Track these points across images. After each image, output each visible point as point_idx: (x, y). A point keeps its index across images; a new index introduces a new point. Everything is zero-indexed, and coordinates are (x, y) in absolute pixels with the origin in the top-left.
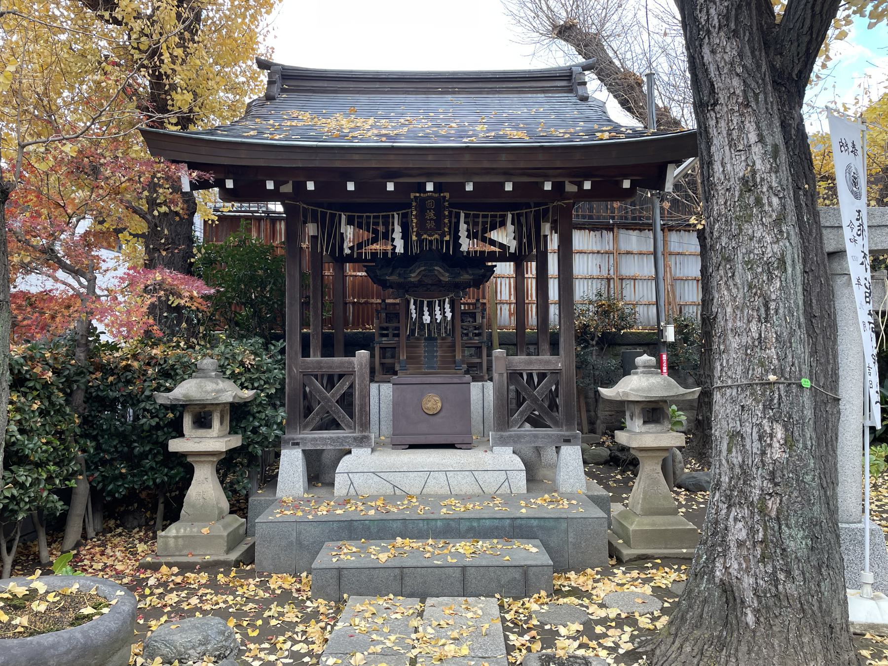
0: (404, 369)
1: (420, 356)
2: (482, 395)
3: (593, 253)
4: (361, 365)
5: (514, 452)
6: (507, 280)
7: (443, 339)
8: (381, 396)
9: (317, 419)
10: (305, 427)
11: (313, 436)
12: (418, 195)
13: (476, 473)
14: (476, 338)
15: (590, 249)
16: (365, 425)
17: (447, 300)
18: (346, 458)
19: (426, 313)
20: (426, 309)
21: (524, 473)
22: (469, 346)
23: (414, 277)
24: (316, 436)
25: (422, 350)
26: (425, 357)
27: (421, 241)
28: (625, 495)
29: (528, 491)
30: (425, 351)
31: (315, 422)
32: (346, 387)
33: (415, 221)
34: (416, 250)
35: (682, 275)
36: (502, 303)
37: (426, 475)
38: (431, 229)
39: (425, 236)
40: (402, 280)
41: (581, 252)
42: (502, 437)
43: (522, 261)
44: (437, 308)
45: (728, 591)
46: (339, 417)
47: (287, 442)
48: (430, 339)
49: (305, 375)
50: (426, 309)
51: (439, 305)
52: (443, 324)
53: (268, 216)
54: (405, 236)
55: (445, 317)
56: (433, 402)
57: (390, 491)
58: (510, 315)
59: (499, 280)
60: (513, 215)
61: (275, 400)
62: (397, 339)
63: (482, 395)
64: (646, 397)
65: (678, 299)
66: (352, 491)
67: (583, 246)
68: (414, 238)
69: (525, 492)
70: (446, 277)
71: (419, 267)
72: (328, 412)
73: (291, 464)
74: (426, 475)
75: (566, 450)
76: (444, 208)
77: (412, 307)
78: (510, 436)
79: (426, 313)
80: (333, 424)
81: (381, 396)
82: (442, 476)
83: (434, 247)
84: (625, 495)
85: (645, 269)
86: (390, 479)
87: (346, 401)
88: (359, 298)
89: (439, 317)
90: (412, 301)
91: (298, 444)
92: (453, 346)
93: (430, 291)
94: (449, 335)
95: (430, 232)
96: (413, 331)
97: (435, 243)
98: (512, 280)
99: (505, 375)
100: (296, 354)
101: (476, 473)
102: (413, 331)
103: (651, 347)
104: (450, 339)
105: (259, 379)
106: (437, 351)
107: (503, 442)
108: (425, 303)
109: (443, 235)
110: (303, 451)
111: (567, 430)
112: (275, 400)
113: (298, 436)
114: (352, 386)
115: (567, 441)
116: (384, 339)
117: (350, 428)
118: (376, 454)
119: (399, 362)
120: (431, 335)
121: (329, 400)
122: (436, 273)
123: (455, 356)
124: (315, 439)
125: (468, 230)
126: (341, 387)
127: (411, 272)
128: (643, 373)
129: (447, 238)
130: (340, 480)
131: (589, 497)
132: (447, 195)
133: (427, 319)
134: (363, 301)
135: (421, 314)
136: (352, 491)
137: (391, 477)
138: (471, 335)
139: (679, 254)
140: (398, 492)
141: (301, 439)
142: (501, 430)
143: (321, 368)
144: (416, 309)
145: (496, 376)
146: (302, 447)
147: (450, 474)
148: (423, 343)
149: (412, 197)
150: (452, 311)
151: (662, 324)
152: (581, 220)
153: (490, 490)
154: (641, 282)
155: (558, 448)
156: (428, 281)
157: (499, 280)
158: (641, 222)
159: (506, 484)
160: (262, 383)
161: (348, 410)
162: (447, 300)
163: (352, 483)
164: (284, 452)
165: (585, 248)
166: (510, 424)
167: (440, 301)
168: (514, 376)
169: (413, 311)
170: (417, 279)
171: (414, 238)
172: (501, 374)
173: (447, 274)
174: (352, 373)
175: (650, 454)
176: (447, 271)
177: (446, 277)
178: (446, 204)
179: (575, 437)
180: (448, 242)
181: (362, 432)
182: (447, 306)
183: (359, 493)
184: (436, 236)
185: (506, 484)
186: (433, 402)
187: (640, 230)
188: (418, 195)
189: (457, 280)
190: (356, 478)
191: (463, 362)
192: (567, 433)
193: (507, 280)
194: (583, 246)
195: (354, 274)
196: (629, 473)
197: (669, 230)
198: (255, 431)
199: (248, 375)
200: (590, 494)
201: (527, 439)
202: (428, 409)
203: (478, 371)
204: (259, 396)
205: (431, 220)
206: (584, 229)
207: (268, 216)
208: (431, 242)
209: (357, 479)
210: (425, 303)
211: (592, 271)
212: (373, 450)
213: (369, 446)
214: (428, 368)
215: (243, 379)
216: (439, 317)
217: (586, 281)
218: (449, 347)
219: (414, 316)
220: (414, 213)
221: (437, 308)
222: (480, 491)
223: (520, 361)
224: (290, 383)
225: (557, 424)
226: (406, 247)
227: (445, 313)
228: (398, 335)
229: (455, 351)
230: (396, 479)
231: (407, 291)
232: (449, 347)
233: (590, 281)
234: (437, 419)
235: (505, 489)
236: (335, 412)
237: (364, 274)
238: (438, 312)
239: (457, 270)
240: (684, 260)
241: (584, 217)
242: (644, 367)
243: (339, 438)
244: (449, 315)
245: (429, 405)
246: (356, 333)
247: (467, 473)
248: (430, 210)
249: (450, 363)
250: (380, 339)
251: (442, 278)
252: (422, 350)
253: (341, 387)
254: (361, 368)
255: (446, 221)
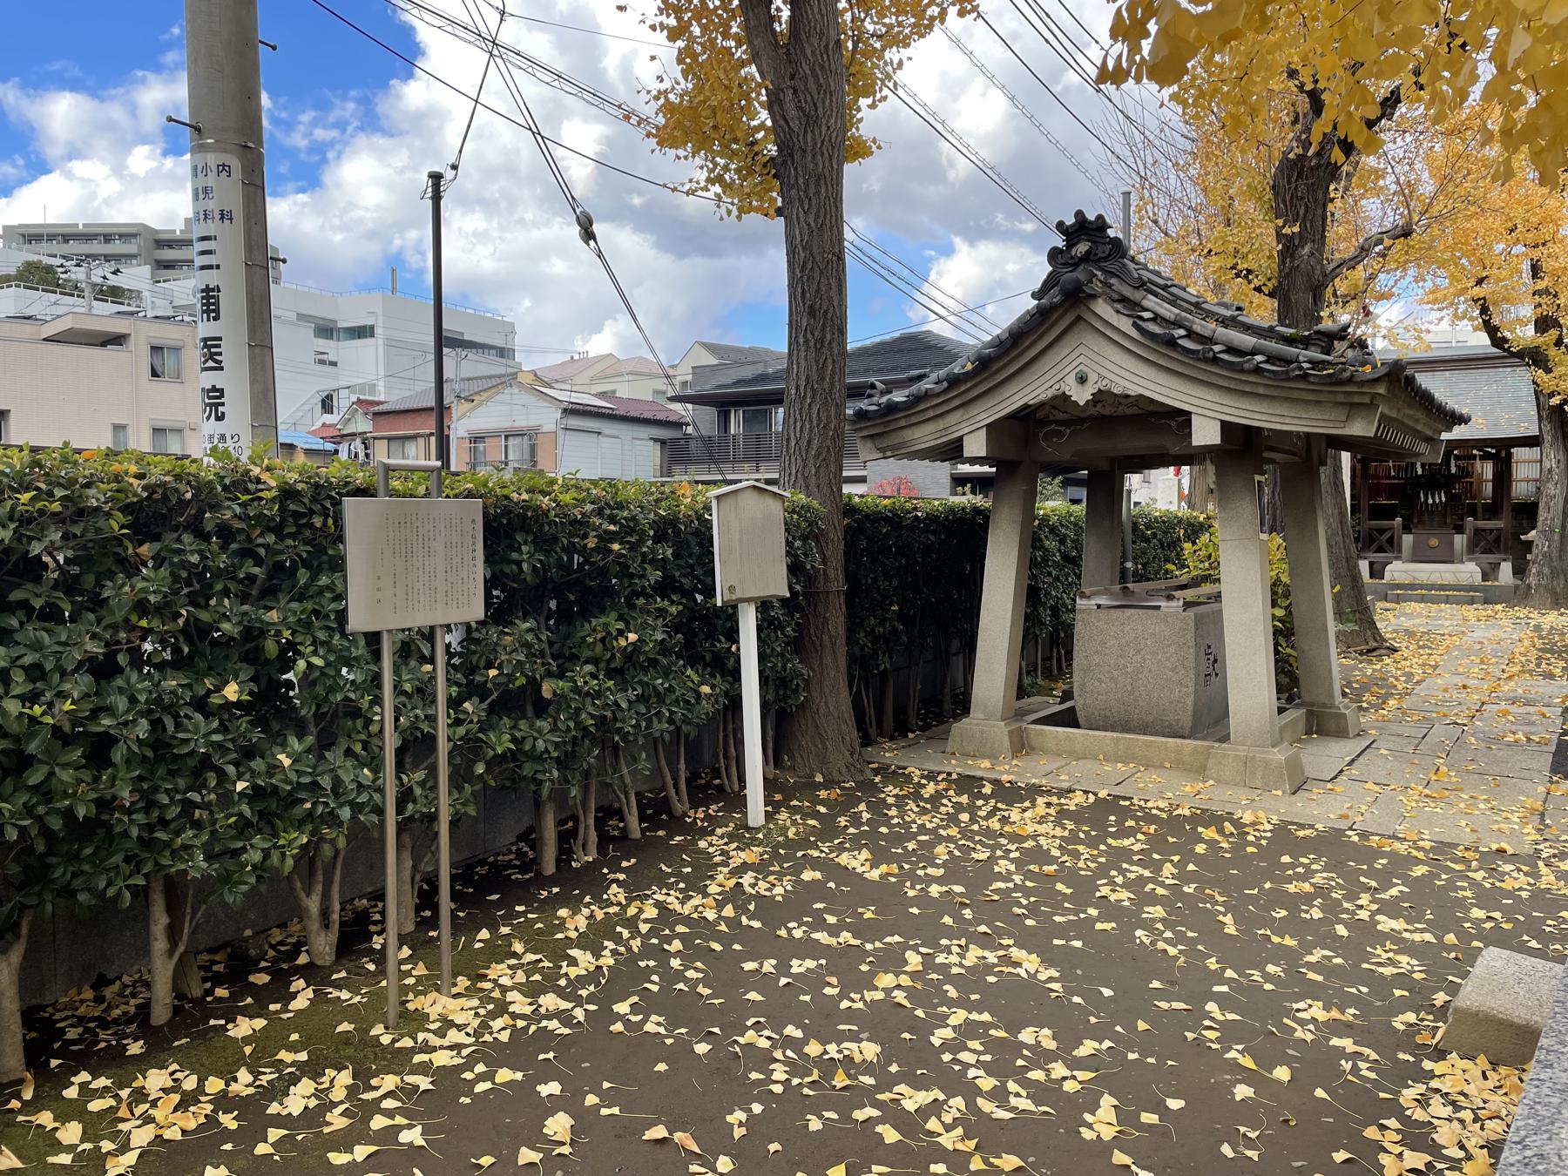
2: (1460, 541)
8: (1407, 540)
16: (1400, 551)
28: (1286, 859)
45: (1529, 587)
56: (1434, 542)
63: (1460, 541)
75: (1503, 564)
81: (1407, 540)
84: (1286, 859)
87: (1390, 541)
107: (1470, 560)
126: (1387, 535)
147: (429, 425)
168: (1477, 531)
203: (1459, 529)
249: (1444, 524)
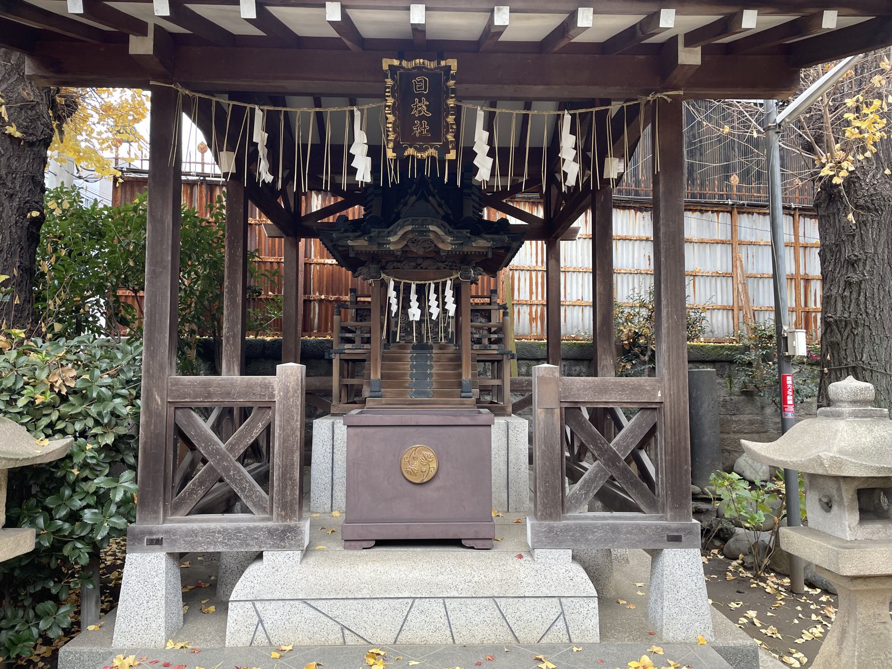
0: (376, 395)
1: (405, 374)
3: (641, 240)
4: (286, 390)
5: (574, 558)
6: (534, 274)
7: (442, 347)
9: (201, 493)
10: (176, 509)
11: (190, 526)
12: (396, 62)
13: (502, 602)
14: (494, 346)
15: (636, 234)
17: (449, 283)
18: (253, 570)
19: (414, 304)
20: (413, 297)
21: (595, 603)
22: (483, 363)
23: (394, 241)
24: (195, 526)
25: (408, 364)
26: (412, 375)
27: (403, 161)
29: (603, 635)
30: (412, 367)
31: (196, 498)
32: (256, 433)
33: (391, 118)
34: (394, 178)
35: (754, 272)
36: (520, 304)
37: (404, 606)
38: (422, 138)
39: (410, 151)
40: (375, 248)
41: (625, 239)
42: (551, 529)
43: (556, 238)
44: (433, 296)
46: (243, 490)
47: (137, 538)
48: (422, 346)
49: (178, 407)
50: (413, 297)
51: (436, 291)
52: (441, 321)
53: (204, 180)
54: (374, 152)
55: (445, 311)
56: (421, 460)
57: (334, 637)
58: (532, 320)
59: (516, 274)
60: (573, 116)
61: (117, 455)
62: (366, 346)
64: (879, 469)
65: (751, 304)
66: (261, 637)
67: (628, 230)
68: (390, 154)
69: (597, 639)
70: (447, 244)
71: (402, 227)
72: (221, 480)
73: (147, 579)
74: (404, 606)
76: (448, 92)
77: (392, 294)
78: (567, 529)
79: (414, 304)
80: (228, 504)
82: (437, 607)
83: (427, 172)
85: (708, 262)
86: (335, 613)
88: (327, 294)
89: (435, 311)
90: (392, 284)
91: (159, 542)
92: (457, 361)
93: (421, 265)
94: (450, 341)
95: (421, 143)
96: (391, 335)
97: (428, 165)
98: (540, 274)
99: (557, 411)
100: (162, 368)
101: (502, 602)
102: (391, 335)
103: (718, 365)
104: (452, 348)
105: (87, 415)
106: (431, 367)
107: (553, 540)
108: (413, 287)
109: (445, 150)
110: (170, 554)
111: (674, 519)
112: (117, 455)
113: (162, 525)
114: (268, 430)
115: (675, 539)
116: (347, 346)
117: (264, 510)
118: (311, 560)
119: (369, 384)
120: (423, 339)
121: (223, 457)
122: (432, 236)
123: (460, 375)
124: (193, 533)
125: (490, 142)
126: (249, 432)
127: (389, 235)
128: (855, 415)
129: (452, 156)
130: (238, 615)
131: (719, 650)
132: (453, 63)
133: (415, 313)
134: (333, 298)
135: (405, 305)
136: (261, 637)
137: (337, 609)
138: (486, 341)
139: (751, 244)
140: (351, 639)
141: (167, 532)
142: (550, 516)
143: (209, 395)
144: (398, 297)
145: (539, 413)
146: (167, 548)
147: (452, 604)
148: (409, 353)
149: (385, 67)
150: (457, 301)
151: (785, 328)
152: (624, 197)
153: (529, 634)
154: (702, 279)
155: (655, 554)
156: (418, 250)
157: (516, 274)
158: (703, 200)
159: (560, 624)
160: (90, 422)
161: (271, 472)
162: (449, 283)
163: (261, 621)
164: (132, 558)
165: (630, 234)
166: (567, 504)
167: (437, 285)
169: (394, 301)
170: (400, 246)
171: (390, 154)
172: (550, 411)
173: (449, 239)
174: (268, 406)
175: (873, 585)
176: (449, 233)
177: (447, 244)
178: (451, 83)
179: (690, 531)
180: (453, 163)
181: (284, 518)
182: (449, 293)
183: (274, 640)
184: (432, 152)
185: (560, 624)
186: (421, 460)
187: (701, 211)
188: (396, 62)
189: (466, 249)
190: (270, 612)
191: (473, 384)
192: (675, 524)
193: (528, 274)
194: (628, 230)
195: (322, 261)
196: (716, 551)
197: (739, 213)
198: (74, 517)
199: (63, 409)
200: (720, 643)
201: (599, 534)
202: (412, 473)
204: (82, 449)
205: (421, 118)
206: (629, 208)
207: (204, 180)
208: (421, 162)
209: (272, 614)
210: (413, 287)
211: (639, 263)
212: (307, 552)
213: (298, 546)
214: (418, 393)
215: (54, 417)
216: (435, 311)
217: (631, 277)
218: (451, 360)
219: (394, 308)
220: (390, 101)
221: (433, 296)
222: (510, 637)
223: (585, 388)
224: (147, 423)
225: (653, 505)
226: (375, 171)
227: (444, 303)
228: (368, 341)
229: (460, 366)
230: (348, 612)
231: (383, 268)
232: (451, 360)
233: (636, 277)
234: (429, 492)
235: (558, 635)
236: (234, 480)
237: (334, 261)
238: (433, 302)
239: (466, 232)
240: (757, 252)
241: (628, 192)
242: (854, 402)
243: (238, 530)
244: (451, 307)
245: (415, 466)
246: (321, 342)
247: (485, 602)
248: (420, 96)
250: (341, 347)
251: (441, 246)
252: (408, 364)
253: (249, 432)
254: (286, 397)
255: (451, 119)
